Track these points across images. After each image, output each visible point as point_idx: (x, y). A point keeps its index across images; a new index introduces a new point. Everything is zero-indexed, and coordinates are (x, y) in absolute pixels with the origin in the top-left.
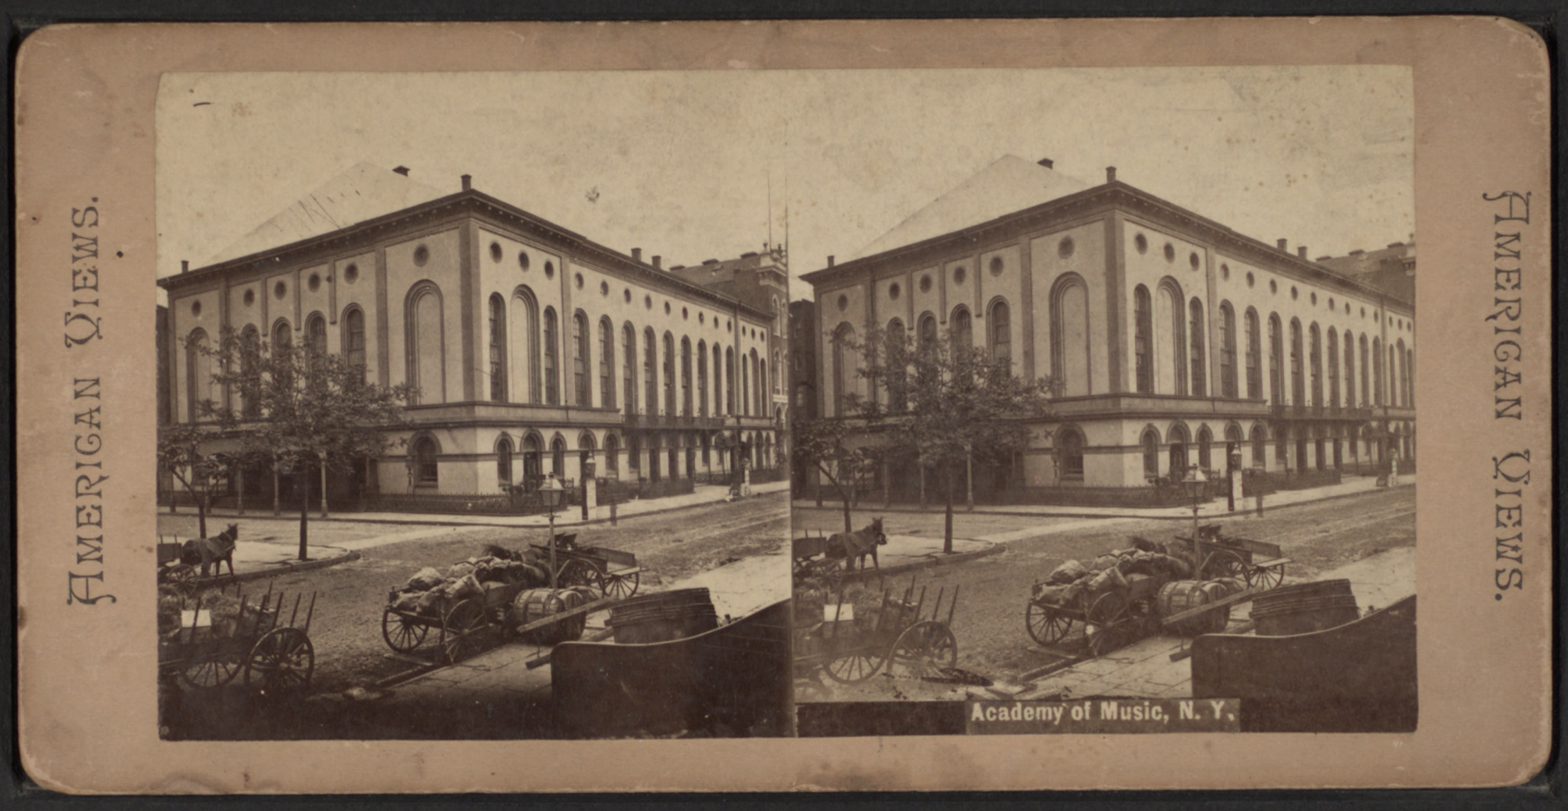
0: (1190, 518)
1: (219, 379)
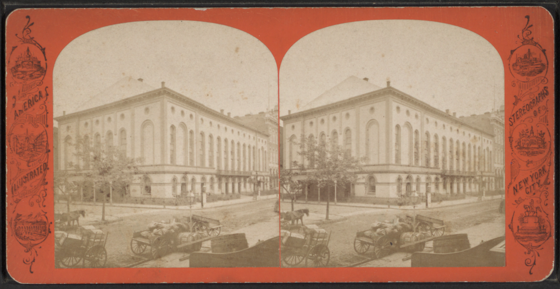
0: (189, 210)
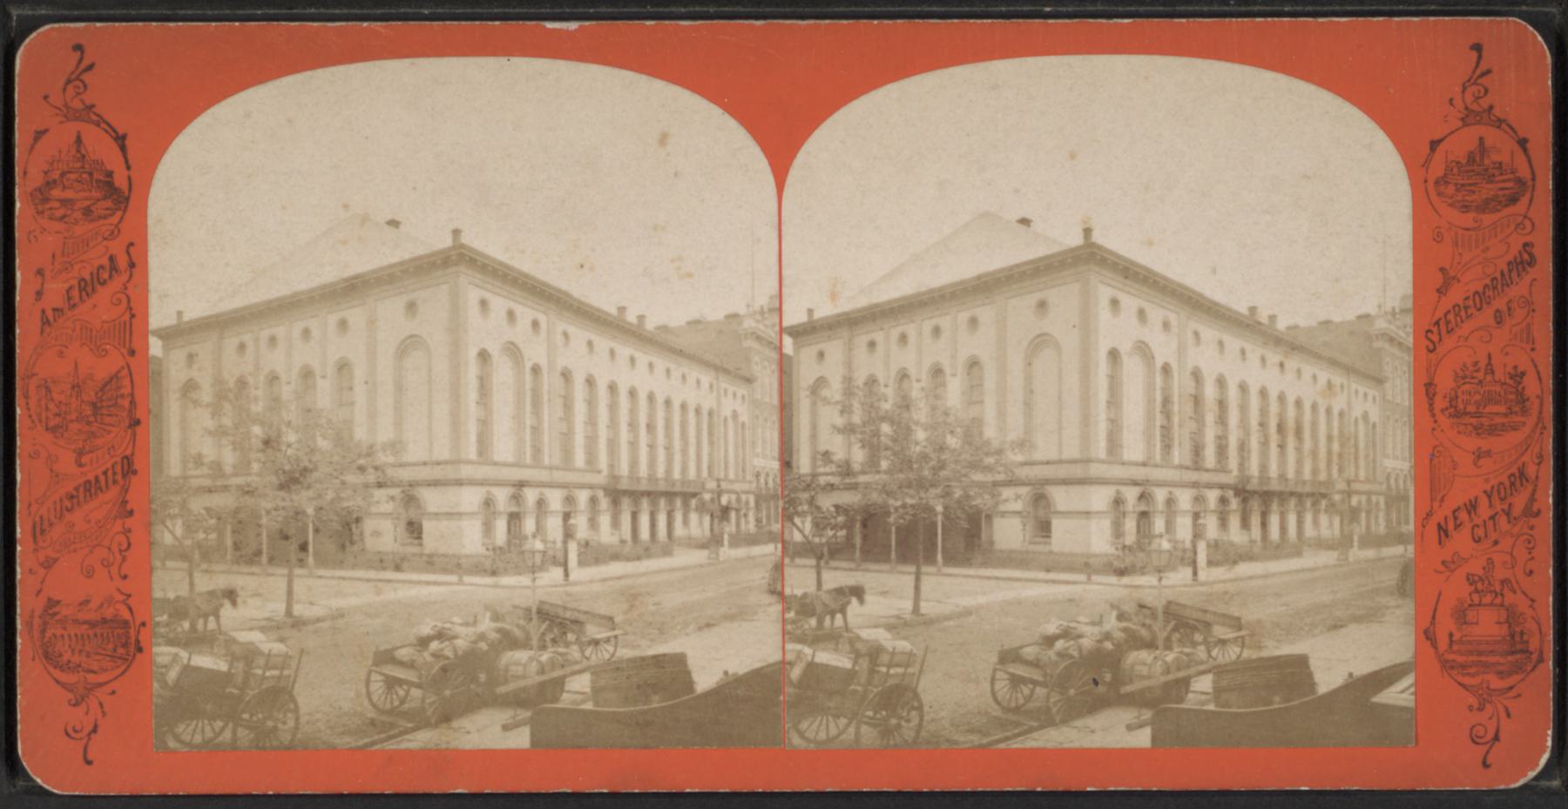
1: (840, 431)
